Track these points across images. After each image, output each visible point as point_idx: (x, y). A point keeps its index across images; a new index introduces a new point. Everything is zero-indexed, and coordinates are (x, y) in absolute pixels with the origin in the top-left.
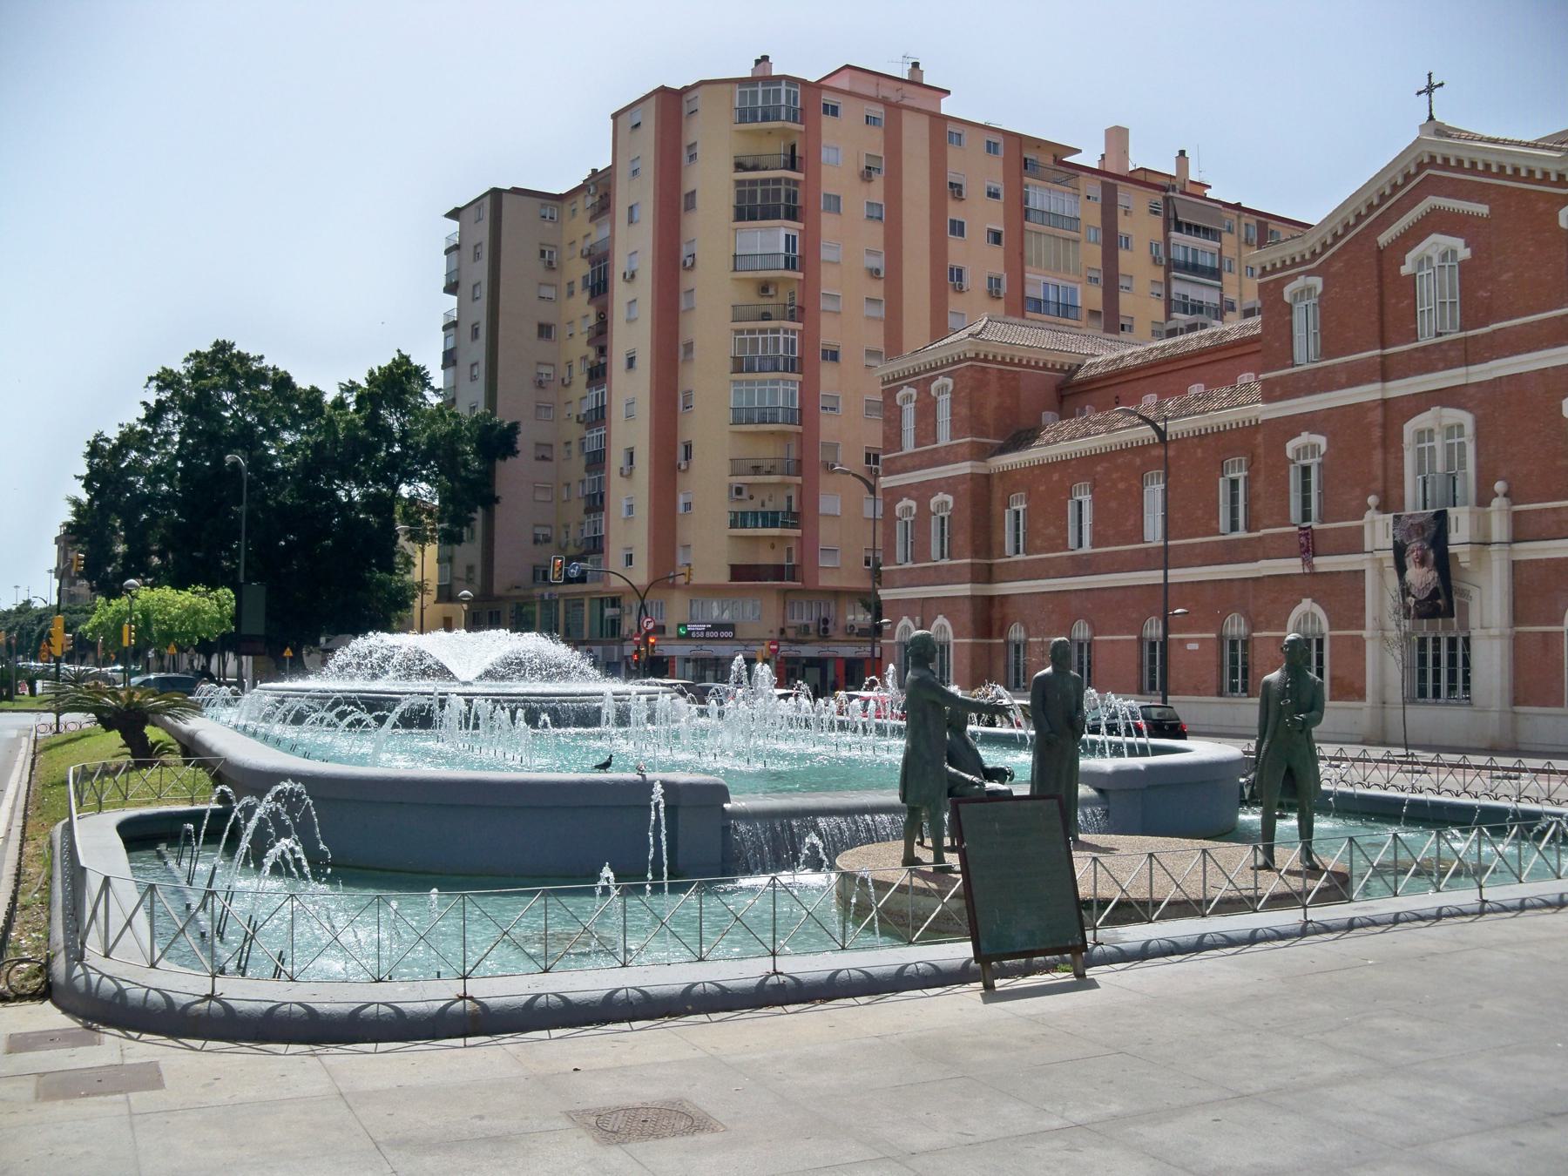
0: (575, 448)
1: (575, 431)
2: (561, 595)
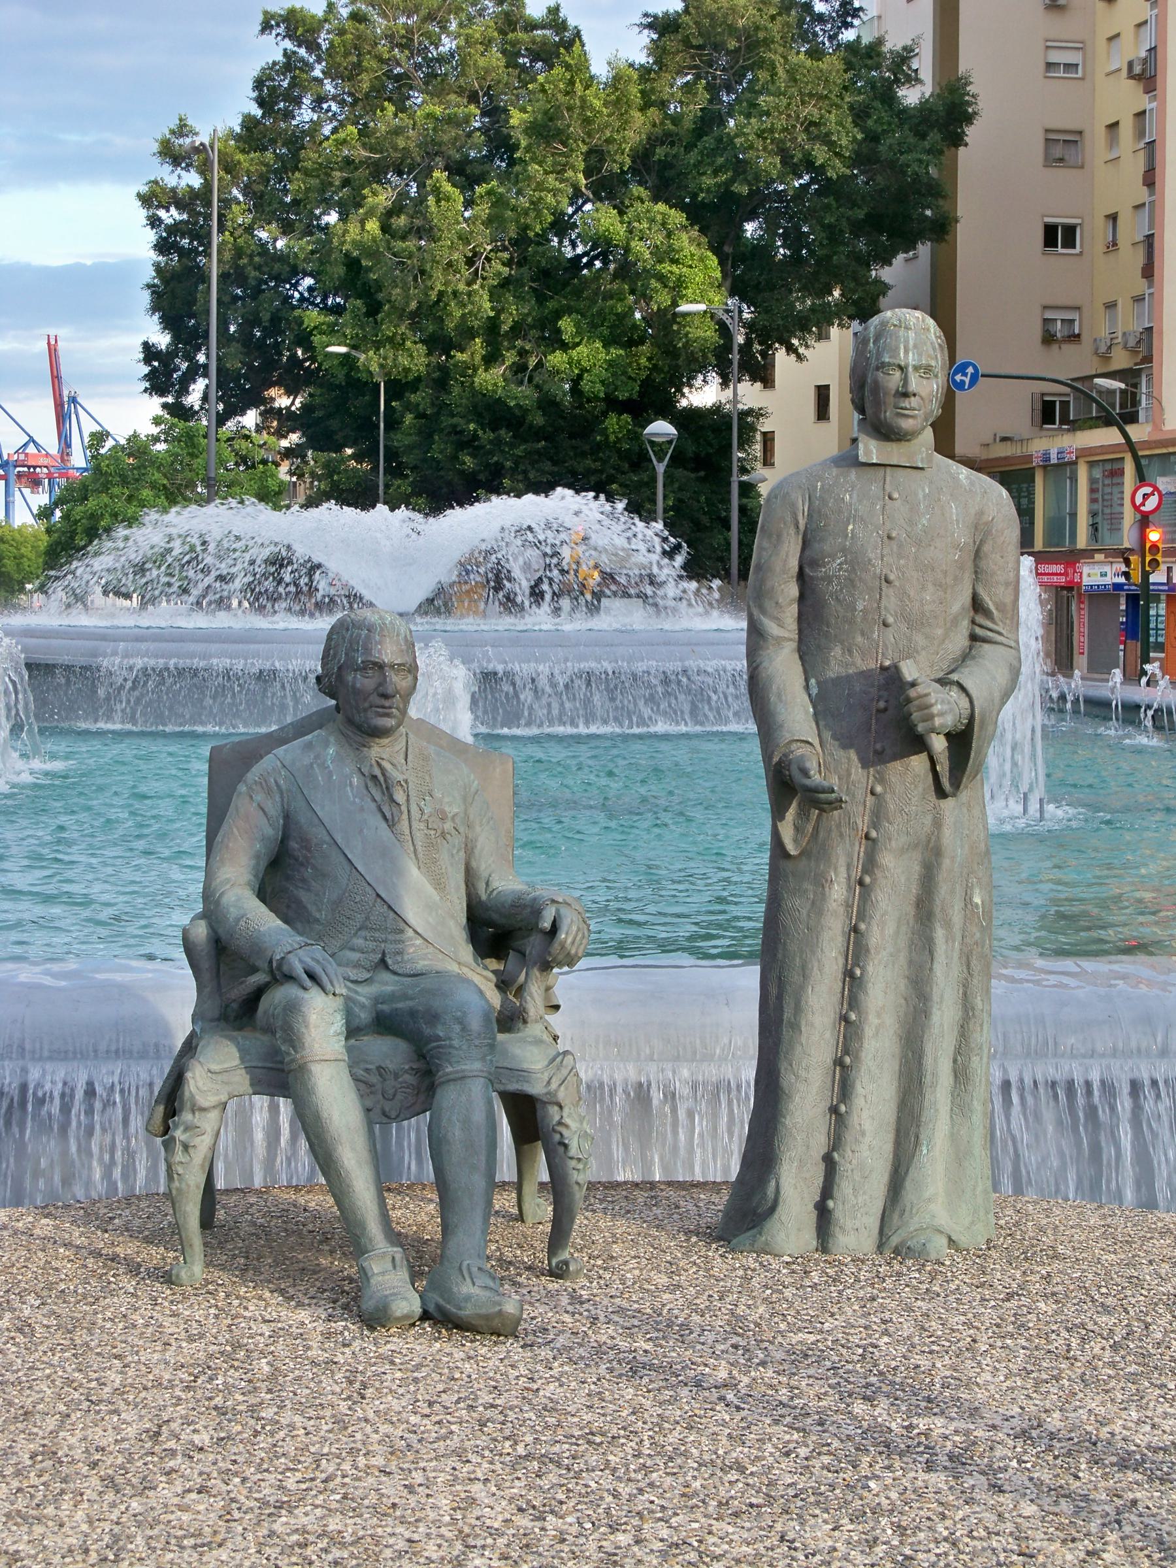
0: (1127, 130)
1: (1123, 99)
2: (1083, 452)
